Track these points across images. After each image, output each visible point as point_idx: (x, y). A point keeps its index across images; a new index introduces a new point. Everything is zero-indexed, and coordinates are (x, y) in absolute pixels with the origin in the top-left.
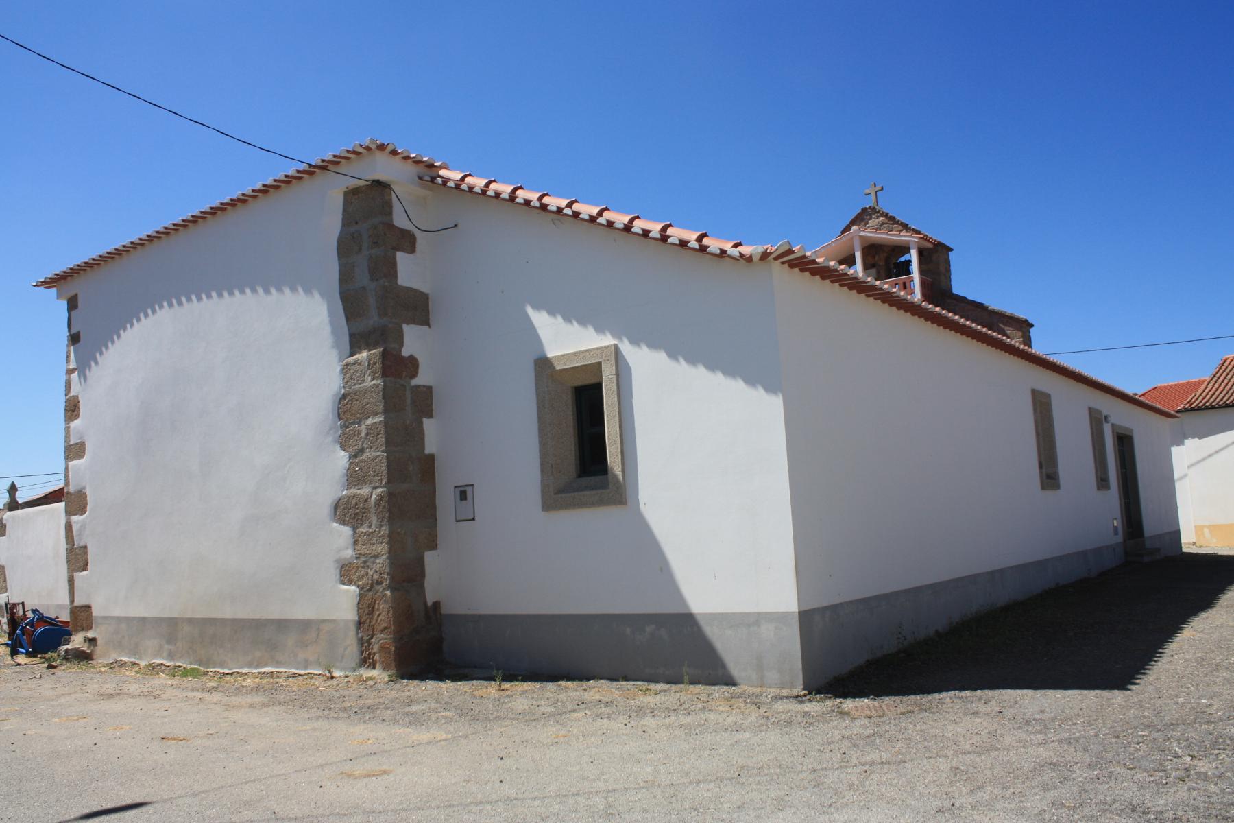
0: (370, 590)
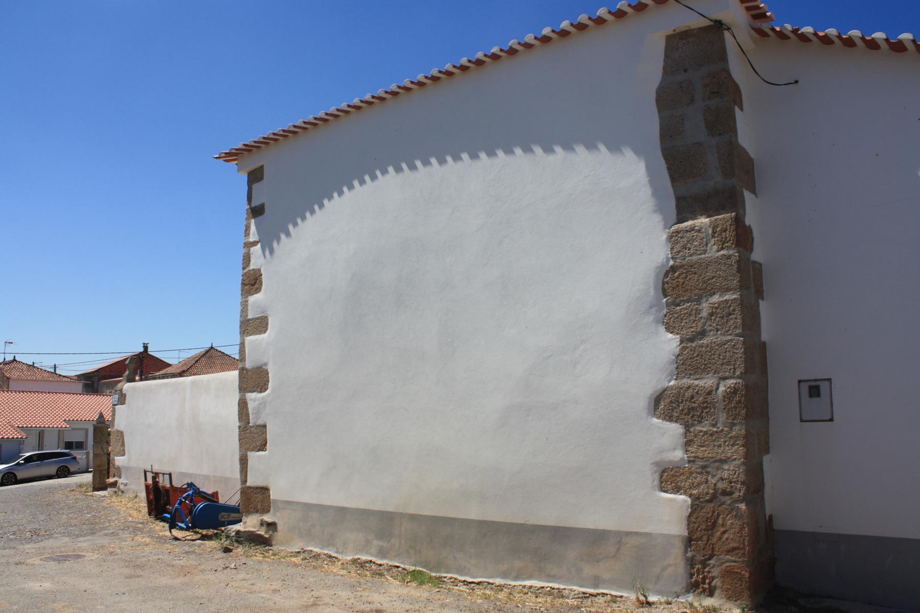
0: (710, 501)
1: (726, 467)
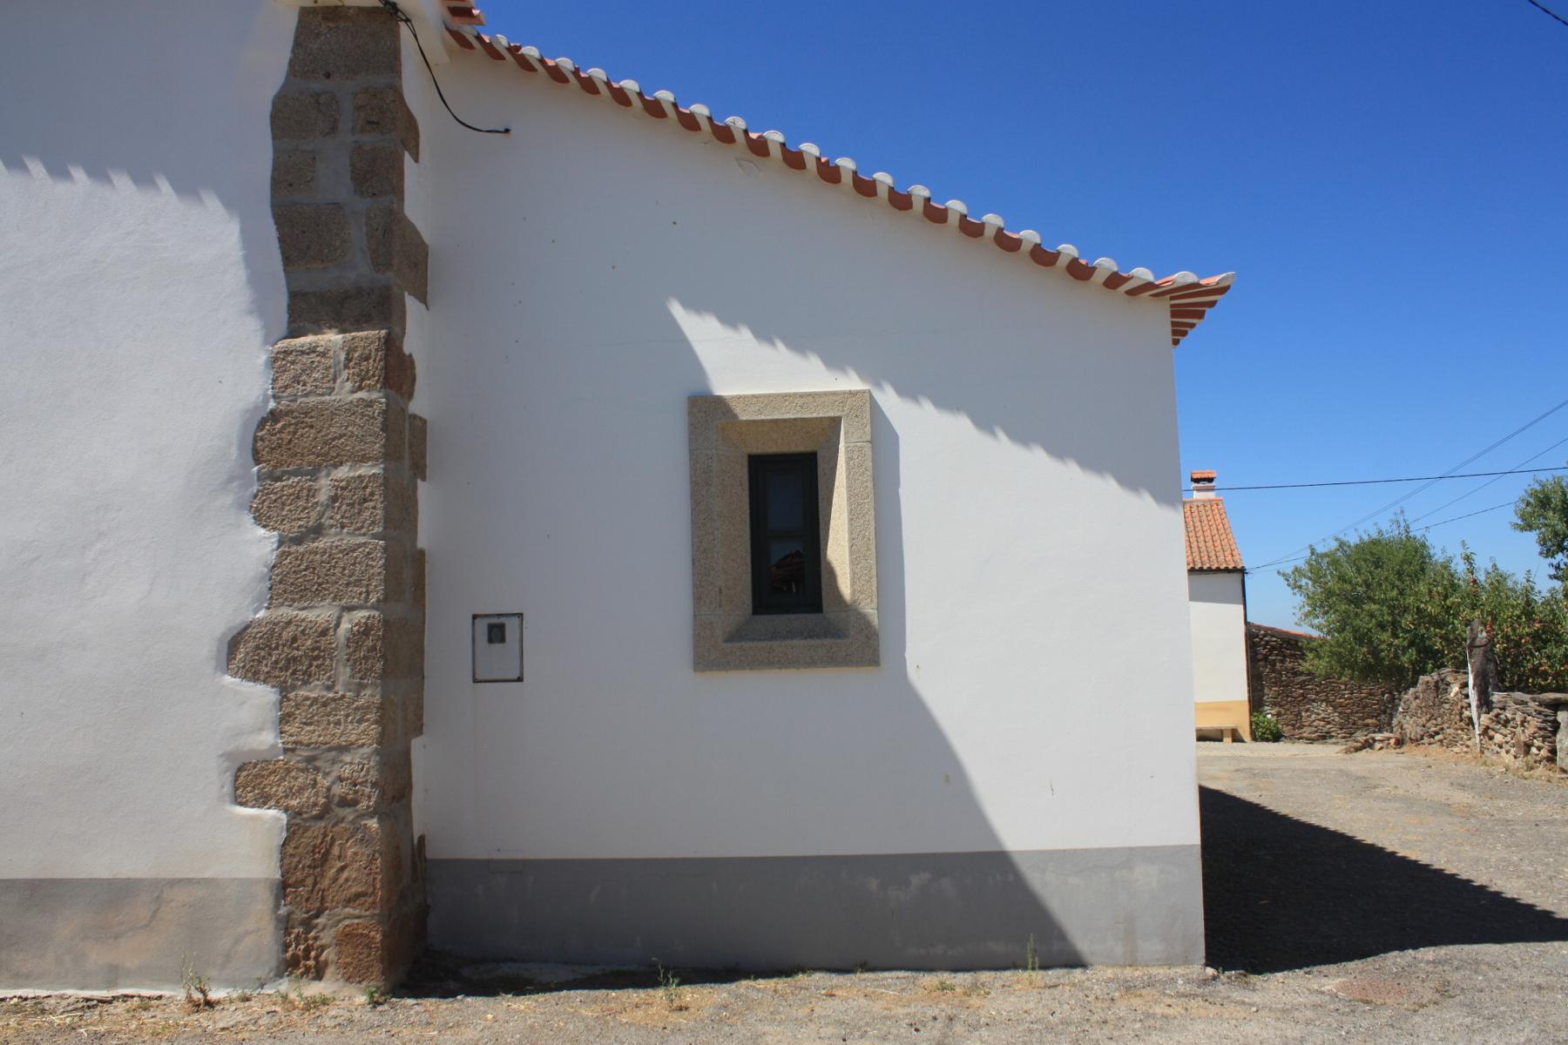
0: (319, 817)
1: (347, 759)
